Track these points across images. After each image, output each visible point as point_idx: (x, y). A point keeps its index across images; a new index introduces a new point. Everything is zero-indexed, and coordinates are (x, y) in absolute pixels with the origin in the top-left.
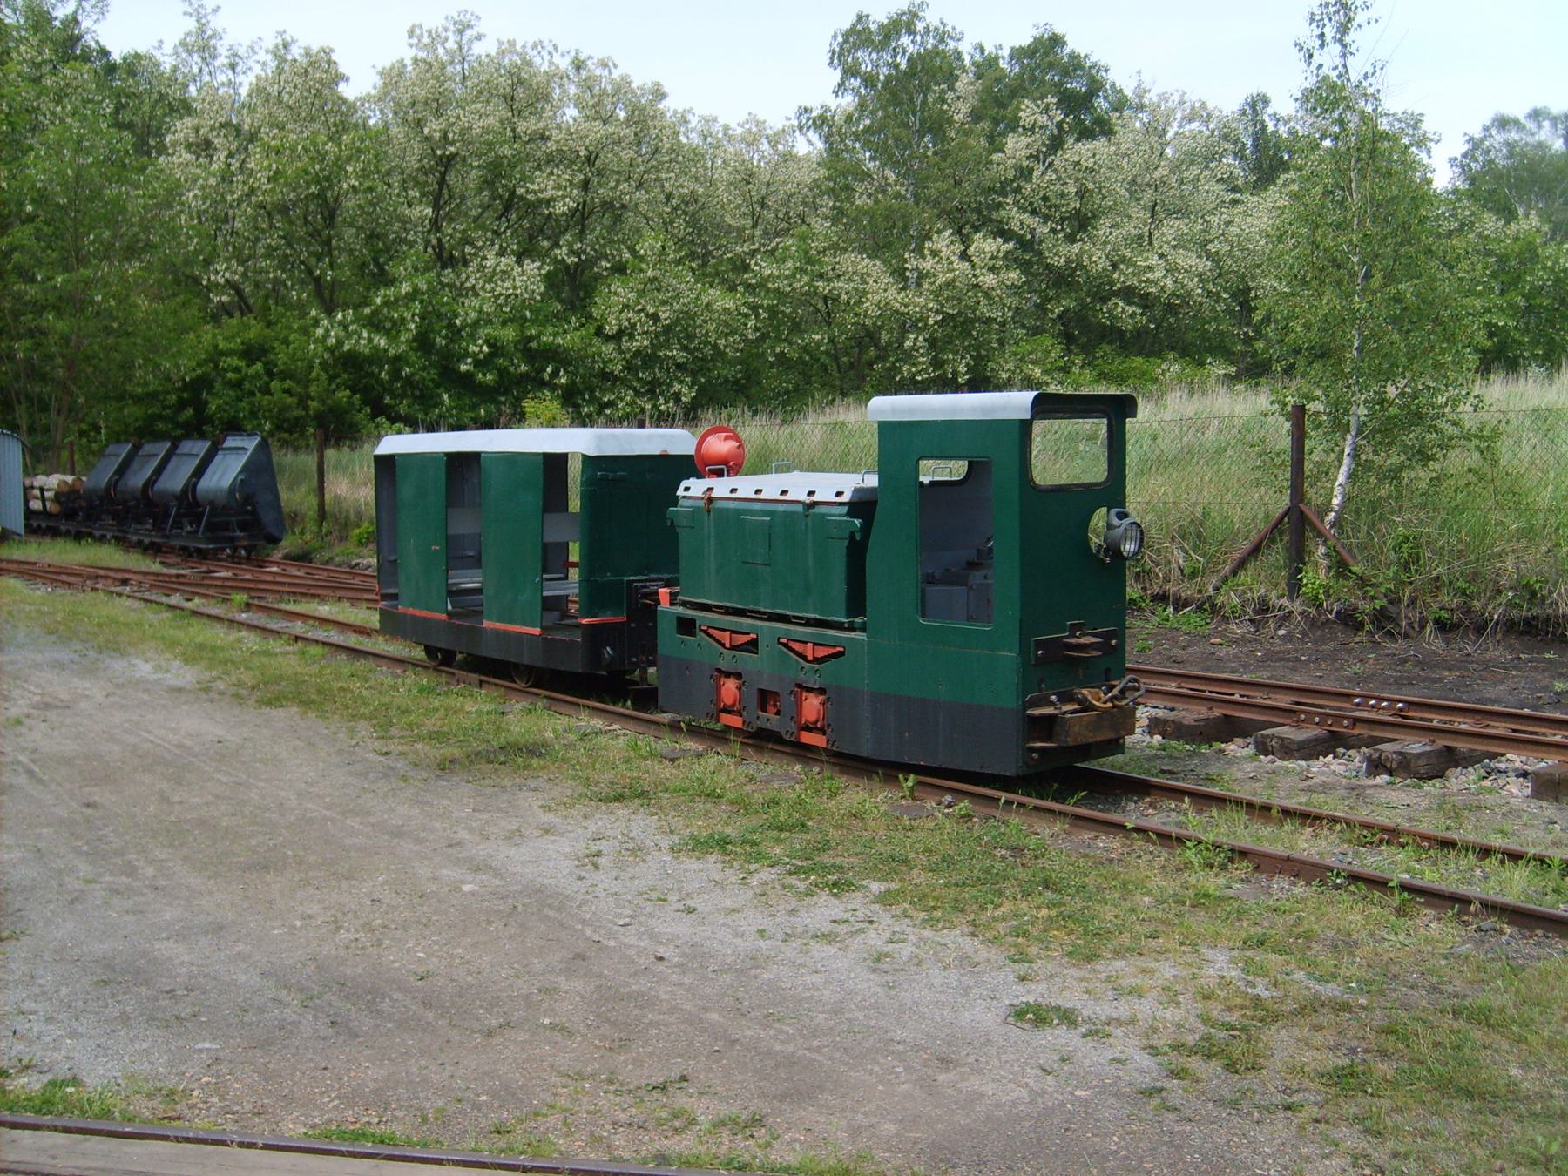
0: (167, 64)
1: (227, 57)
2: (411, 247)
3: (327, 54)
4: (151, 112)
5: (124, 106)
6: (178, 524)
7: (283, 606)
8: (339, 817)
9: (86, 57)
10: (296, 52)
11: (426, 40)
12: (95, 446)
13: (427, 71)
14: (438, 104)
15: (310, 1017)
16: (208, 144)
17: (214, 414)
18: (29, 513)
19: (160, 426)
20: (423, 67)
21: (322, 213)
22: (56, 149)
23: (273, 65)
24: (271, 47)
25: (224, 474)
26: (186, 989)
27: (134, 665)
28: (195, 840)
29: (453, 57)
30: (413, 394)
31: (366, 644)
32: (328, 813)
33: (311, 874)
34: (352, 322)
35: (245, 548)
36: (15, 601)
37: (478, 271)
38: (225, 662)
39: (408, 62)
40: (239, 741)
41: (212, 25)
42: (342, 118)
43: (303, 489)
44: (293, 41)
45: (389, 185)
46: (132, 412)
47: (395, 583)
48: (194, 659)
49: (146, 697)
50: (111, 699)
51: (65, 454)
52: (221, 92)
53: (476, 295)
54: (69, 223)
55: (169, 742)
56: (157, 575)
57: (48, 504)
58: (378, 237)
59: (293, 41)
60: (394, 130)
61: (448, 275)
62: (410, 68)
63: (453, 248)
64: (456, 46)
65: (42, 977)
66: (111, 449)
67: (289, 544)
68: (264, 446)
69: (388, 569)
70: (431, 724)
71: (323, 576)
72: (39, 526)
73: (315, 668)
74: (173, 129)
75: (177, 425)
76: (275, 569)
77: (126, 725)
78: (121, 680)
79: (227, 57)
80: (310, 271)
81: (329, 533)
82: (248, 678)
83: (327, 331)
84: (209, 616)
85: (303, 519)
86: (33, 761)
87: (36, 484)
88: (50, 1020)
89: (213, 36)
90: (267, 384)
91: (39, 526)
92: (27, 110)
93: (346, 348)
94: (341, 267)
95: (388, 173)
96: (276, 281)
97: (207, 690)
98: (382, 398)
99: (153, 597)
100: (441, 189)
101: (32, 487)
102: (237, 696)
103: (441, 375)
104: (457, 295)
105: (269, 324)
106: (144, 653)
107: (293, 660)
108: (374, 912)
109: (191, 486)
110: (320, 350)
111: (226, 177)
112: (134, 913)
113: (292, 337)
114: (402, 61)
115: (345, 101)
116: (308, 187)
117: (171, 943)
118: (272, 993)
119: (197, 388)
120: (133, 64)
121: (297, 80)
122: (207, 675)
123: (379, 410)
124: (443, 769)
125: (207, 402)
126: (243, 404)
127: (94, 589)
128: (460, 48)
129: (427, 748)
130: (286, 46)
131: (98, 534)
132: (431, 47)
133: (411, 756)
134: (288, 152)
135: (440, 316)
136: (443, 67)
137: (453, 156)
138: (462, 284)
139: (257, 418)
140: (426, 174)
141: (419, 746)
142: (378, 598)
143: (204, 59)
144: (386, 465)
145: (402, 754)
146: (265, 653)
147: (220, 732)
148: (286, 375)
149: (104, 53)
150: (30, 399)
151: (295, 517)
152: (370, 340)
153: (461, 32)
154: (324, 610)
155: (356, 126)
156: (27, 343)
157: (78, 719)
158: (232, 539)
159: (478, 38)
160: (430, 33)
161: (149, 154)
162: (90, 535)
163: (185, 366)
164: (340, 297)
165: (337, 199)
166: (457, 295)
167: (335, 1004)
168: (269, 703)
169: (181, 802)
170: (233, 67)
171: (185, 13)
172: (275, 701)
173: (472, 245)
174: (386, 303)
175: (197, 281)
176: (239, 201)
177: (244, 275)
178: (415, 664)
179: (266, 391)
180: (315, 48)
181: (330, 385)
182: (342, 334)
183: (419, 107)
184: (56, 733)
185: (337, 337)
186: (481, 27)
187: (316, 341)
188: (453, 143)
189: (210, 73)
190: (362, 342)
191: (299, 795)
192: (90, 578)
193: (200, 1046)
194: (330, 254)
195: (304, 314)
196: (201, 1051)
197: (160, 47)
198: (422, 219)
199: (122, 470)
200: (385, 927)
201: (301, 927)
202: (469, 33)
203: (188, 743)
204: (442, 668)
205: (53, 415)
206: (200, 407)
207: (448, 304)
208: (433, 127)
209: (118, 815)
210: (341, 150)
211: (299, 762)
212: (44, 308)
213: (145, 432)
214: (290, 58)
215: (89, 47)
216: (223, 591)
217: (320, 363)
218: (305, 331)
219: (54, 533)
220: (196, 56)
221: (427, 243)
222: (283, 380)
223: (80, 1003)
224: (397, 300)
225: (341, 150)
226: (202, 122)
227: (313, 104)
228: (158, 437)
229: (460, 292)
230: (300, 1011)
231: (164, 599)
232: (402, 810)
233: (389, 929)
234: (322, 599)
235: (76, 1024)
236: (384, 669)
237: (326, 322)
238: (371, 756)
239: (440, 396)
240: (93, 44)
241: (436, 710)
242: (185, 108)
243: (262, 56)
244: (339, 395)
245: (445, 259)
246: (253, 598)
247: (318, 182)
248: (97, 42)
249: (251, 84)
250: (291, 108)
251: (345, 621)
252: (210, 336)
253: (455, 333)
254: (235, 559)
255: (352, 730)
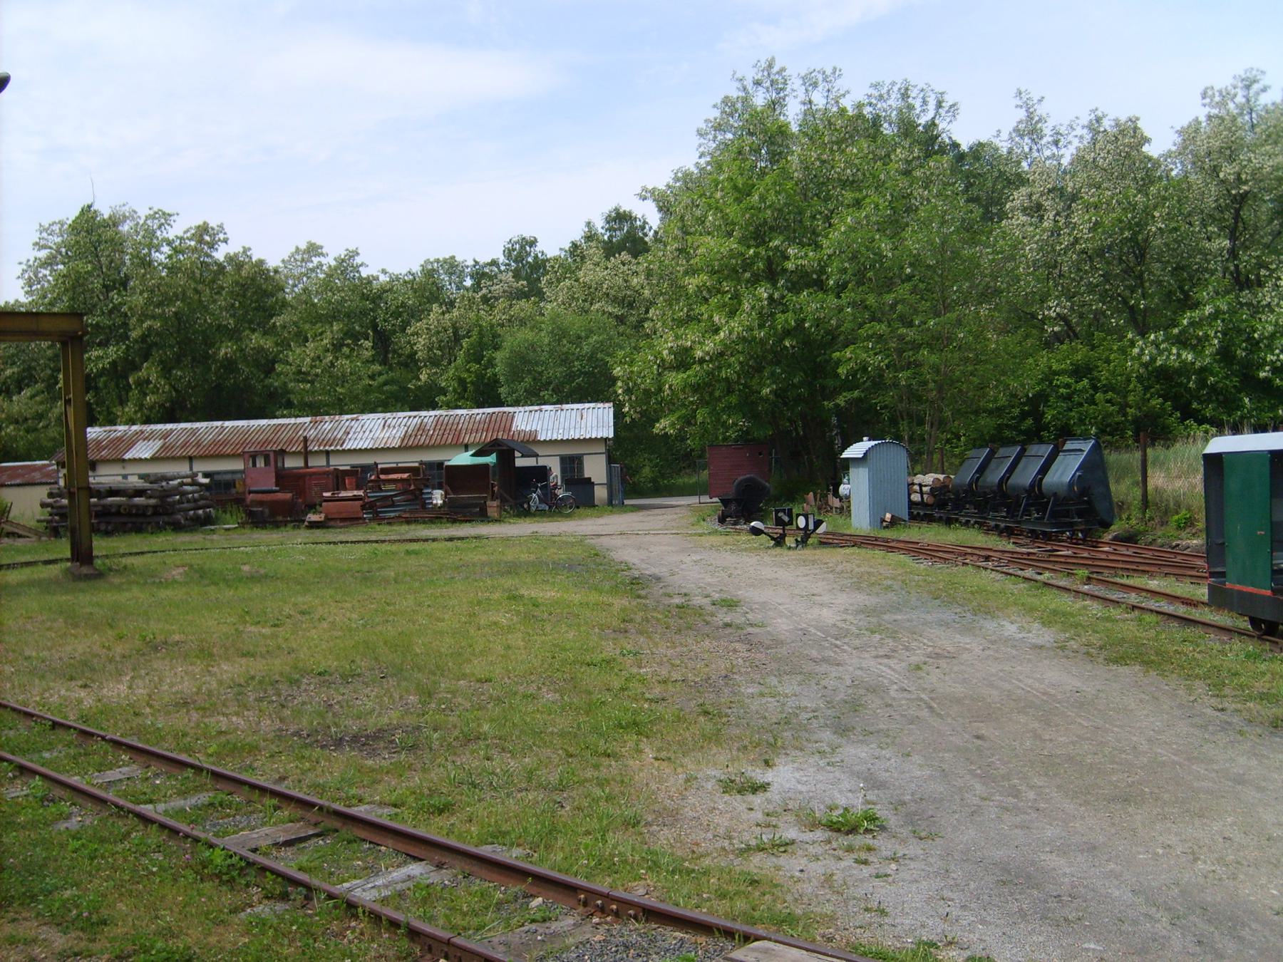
0: (1004, 147)
1: (1051, 136)
2: (1212, 275)
3: (1134, 122)
4: (993, 187)
5: (972, 185)
6: (1027, 512)
7: (1118, 580)
8: (1186, 763)
9: (942, 151)
10: (1107, 124)
11: (1217, 99)
12: (957, 451)
13: (1220, 125)
14: (1231, 152)
15: (1178, 934)
16: (1039, 207)
17: (1049, 423)
18: (912, 504)
19: (1007, 433)
20: (1216, 122)
21: (1134, 253)
22: (926, 224)
23: (1088, 137)
24: (1086, 123)
25: (1065, 471)
26: (1070, 896)
27: (1002, 626)
28: (1066, 772)
29: (1242, 109)
30: (1217, 399)
31: (1195, 614)
32: (1176, 759)
33: (1166, 809)
34: (1163, 341)
35: (1082, 531)
36: (906, 572)
37: (1273, 290)
38: (1076, 626)
39: (1202, 118)
40: (1093, 692)
41: (1038, 112)
42: (1148, 173)
43: (1128, 482)
44: (1104, 116)
45: (1190, 224)
46: (985, 422)
47: (1223, 563)
48: (1050, 622)
49: (1014, 652)
50: (987, 652)
51: (936, 457)
52: (1048, 162)
53: (1272, 311)
54: (937, 279)
55: (1037, 690)
56: (1013, 553)
57: (925, 497)
58: (1183, 268)
59: (1104, 116)
60: (1192, 178)
61: (1246, 296)
62: (1204, 124)
63: (1249, 272)
64: (1243, 100)
65: (954, 872)
66: (970, 453)
67: (1117, 528)
68: (1096, 448)
69: (1216, 551)
70: (1260, 686)
71: (1149, 554)
72: (918, 513)
73: (1152, 633)
74: (1011, 198)
75: (1021, 432)
76: (1106, 549)
77: (1001, 674)
78: (993, 638)
79: (1051, 136)
80: (1125, 302)
81: (1151, 519)
82: (1095, 639)
83: (1142, 350)
84: (1058, 587)
85: (1128, 508)
86: (932, 699)
87: (916, 481)
88: (964, 907)
89: (1039, 121)
90: (1093, 396)
91: (918, 513)
92: (903, 197)
93: (1159, 363)
94: (1152, 296)
95: (1190, 214)
96: (1096, 312)
97: (1063, 648)
98: (1190, 403)
99: (1011, 571)
100: (1236, 222)
101: (913, 484)
102: (1087, 653)
103: (1241, 382)
104: (1255, 313)
105: (1093, 348)
106: (1009, 617)
107: (1132, 626)
108: (1226, 849)
109: (1037, 482)
110: (1136, 366)
111: (1056, 231)
112: (1022, 828)
113: (1112, 357)
114: (1196, 120)
115: (1150, 159)
116: (1122, 234)
117: (1053, 856)
118: (1144, 909)
119: (1036, 404)
120: (978, 151)
121: (1109, 147)
122: (1062, 636)
123: (1187, 413)
124: (1276, 727)
125: (1044, 413)
126: (1073, 414)
127: (964, 564)
128: (1248, 101)
129: (1259, 707)
130: (1098, 120)
131: (963, 520)
132: (1223, 104)
133: (1244, 713)
134: (1104, 206)
135: (1239, 331)
136: (1234, 119)
137: (1247, 193)
138: (1259, 302)
139: (1085, 424)
140: (1222, 212)
141: (1251, 705)
142: (1207, 575)
143: (1033, 140)
144: (1214, 463)
145: (1237, 710)
146: (1108, 619)
147: (1077, 683)
148: (1108, 388)
149: (955, 145)
150: (910, 416)
151: (1122, 506)
152: (1179, 355)
153: (1248, 87)
154: (1153, 584)
155: (1160, 178)
156: (908, 373)
157: (963, 667)
158: (1071, 525)
159: (1264, 90)
160: (1220, 92)
161: (991, 219)
162: (957, 520)
163: (1028, 385)
164: (1151, 320)
165: (1146, 240)
166: (1255, 313)
167: (1200, 925)
168: (1116, 661)
169: (1051, 740)
170: (1056, 143)
171: (1017, 106)
172: (1121, 660)
173: (1267, 268)
174: (1192, 324)
175: (1034, 316)
176: (1066, 250)
177: (1072, 309)
178: (1241, 633)
179: (1092, 402)
180: (1123, 119)
181: (1145, 394)
182: (1155, 352)
183: (1214, 156)
184: (947, 678)
185: (1151, 354)
186: (1265, 81)
187: (1133, 359)
188: (1246, 182)
189: (1038, 151)
190: (1172, 358)
191: (1149, 740)
192: (960, 555)
193: (1086, 945)
194: (1142, 285)
195: (1122, 338)
196: (1087, 950)
197: (998, 136)
198: (1221, 249)
199: (982, 469)
200: (1238, 863)
201: (1163, 855)
202: (1256, 87)
203: (1053, 692)
204: (1265, 637)
205: (927, 427)
206: (1038, 416)
207: (1246, 321)
208: (1227, 171)
209: (1002, 747)
210: (1149, 200)
211: (1145, 712)
212: (920, 346)
213: (997, 440)
214: (1102, 129)
215: (944, 143)
216: (1068, 567)
217: (1137, 377)
218: (1123, 351)
219: (929, 519)
220: (1026, 138)
221: (1226, 270)
222: (1106, 392)
223: (986, 897)
224: (1201, 320)
225: (1149, 200)
226: (1034, 190)
227: (1123, 164)
228: (1009, 442)
229: (1256, 309)
230: (1169, 928)
231: (1020, 573)
232: (1242, 760)
233: (1242, 865)
234: (1152, 575)
235: (984, 914)
236: (1212, 636)
237: (1141, 343)
238: (1209, 711)
239: (1241, 400)
240: (947, 141)
241: (1263, 674)
242: (1021, 180)
243: (1079, 131)
244: (1153, 402)
245: (1242, 282)
246: (1092, 573)
247: (1130, 229)
248: (950, 138)
249: (1072, 155)
250: (1105, 170)
251: (1173, 593)
252: (1045, 359)
253: (1254, 345)
254: (1073, 541)
255: (1189, 689)
